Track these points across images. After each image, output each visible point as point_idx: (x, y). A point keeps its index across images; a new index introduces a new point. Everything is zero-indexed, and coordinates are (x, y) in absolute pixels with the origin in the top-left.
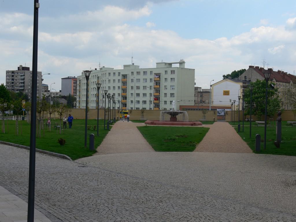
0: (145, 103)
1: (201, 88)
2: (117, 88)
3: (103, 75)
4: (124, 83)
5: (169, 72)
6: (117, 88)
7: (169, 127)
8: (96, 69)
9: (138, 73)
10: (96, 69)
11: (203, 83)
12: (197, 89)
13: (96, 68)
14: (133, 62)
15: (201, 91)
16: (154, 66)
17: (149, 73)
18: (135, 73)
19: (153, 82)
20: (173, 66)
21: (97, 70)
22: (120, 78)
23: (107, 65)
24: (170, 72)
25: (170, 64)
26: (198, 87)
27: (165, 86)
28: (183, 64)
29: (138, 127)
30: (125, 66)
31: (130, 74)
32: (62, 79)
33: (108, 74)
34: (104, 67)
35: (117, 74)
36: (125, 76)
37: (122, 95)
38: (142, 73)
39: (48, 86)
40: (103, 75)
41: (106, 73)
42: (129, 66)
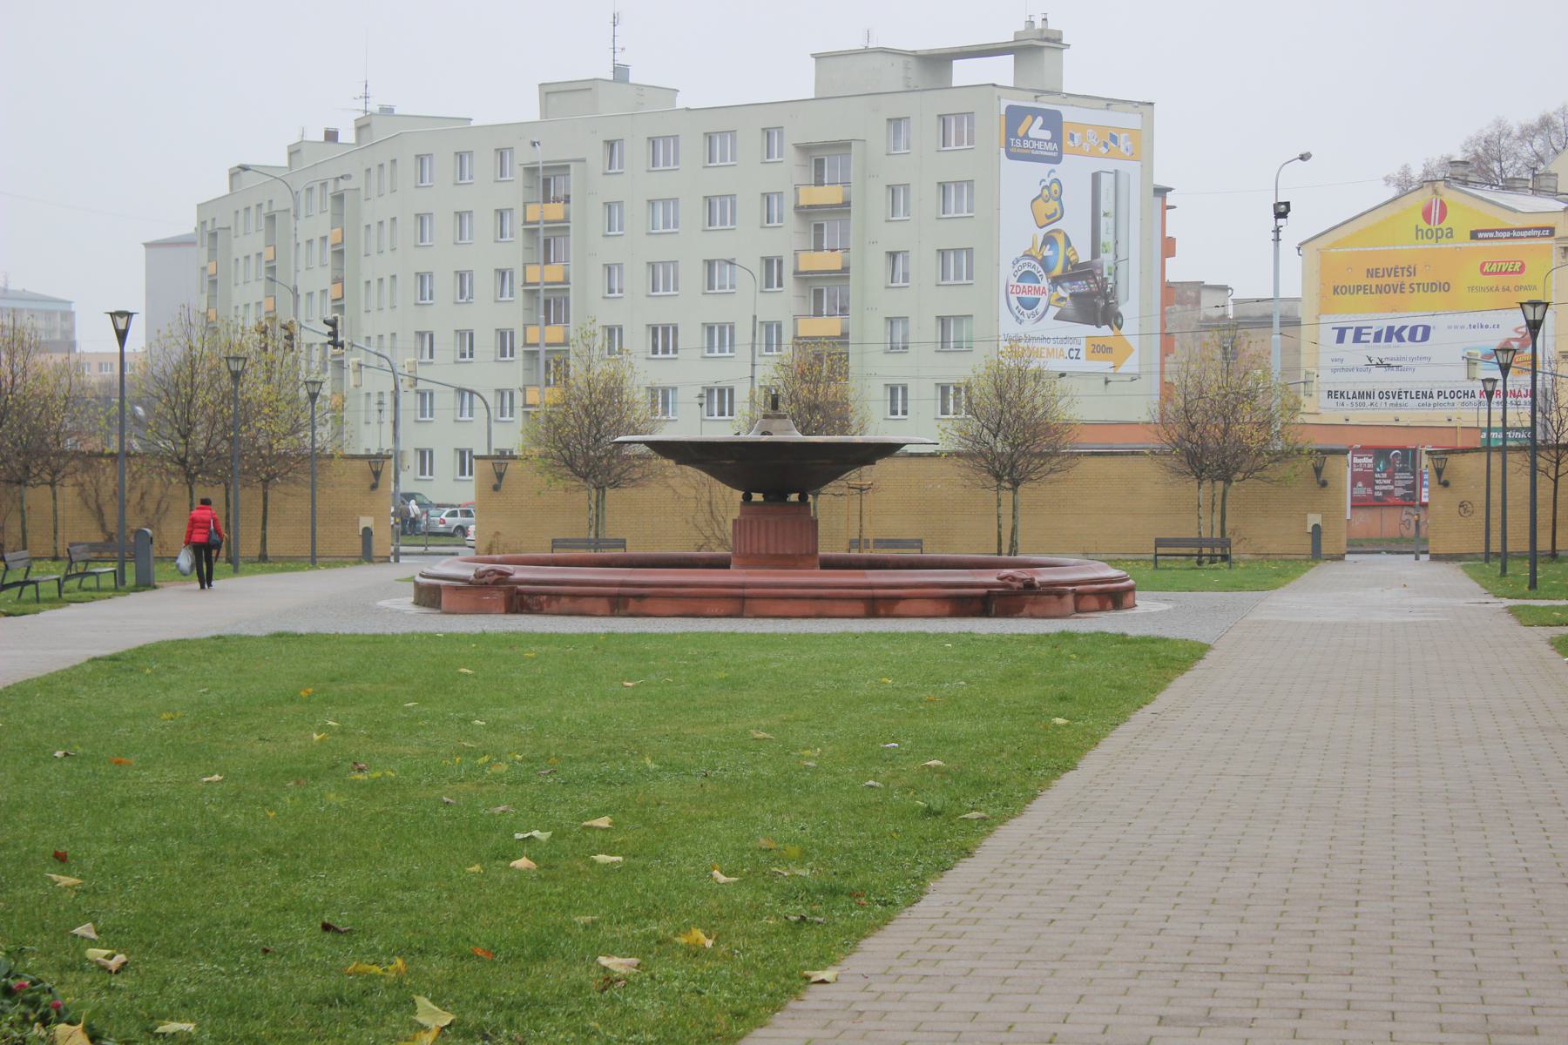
0: (722, 413)
1: (1224, 289)
2: (484, 283)
3: (375, 171)
4: (546, 241)
5: (924, 130)
6: (484, 283)
7: (955, 638)
8: (331, 136)
9: (661, 148)
10: (331, 136)
11: (1229, 251)
12: (1197, 302)
13: (332, 126)
14: (621, 60)
15: (1224, 317)
16: (802, 84)
17: (750, 143)
18: (635, 153)
19: (791, 155)
20: (964, 73)
21: (340, 140)
22: (512, 193)
23: (415, 98)
24: (934, 126)
25: (937, 63)
26: (1199, 286)
27: (891, 321)
28: (1048, 54)
29: (1551, 642)
30: (549, 92)
31: (596, 156)
32: (147, 245)
33: (408, 168)
34: (387, 111)
35: (483, 164)
36: (546, 181)
37: (525, 345)
38: (692, 148)
39: (72, 314)
40: (375, 171)
41: (394, 161)
42: (583, 88)
